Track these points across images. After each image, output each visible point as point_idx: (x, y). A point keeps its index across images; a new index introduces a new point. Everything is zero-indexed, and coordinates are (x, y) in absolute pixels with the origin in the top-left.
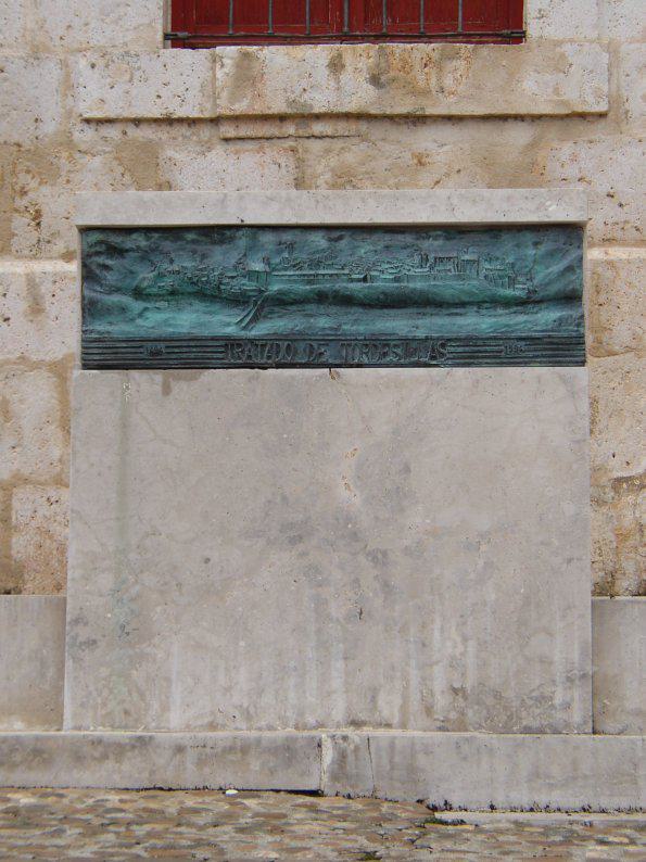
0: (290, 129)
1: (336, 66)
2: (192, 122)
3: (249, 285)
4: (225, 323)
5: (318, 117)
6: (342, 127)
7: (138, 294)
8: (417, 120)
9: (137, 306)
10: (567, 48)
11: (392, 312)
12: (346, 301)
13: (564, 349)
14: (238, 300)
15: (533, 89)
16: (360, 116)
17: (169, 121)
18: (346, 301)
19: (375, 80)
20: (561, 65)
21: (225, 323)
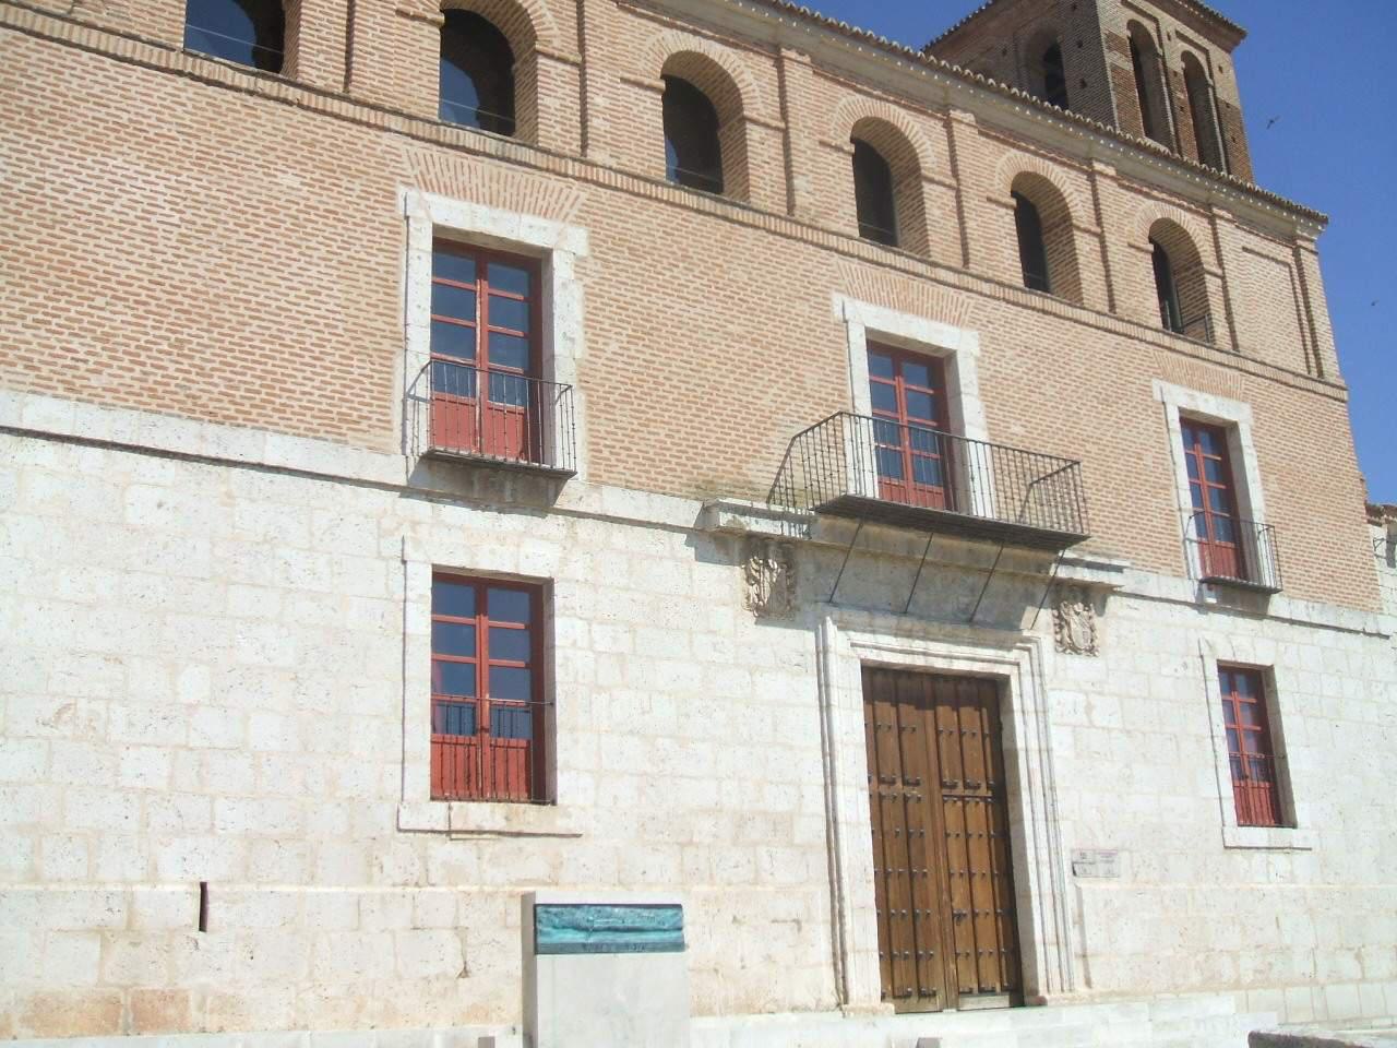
0: (476, 836)
1: (493, 812)
2: (440, 832)
3: (588, 925)
4: (580, 937)
5: (485, 832)
6: (493, 836)
7: (555, 927)
8: (519, 834)
9: (554, 931)
10: (570, 809)
11: (1025, 961)
12: (616, 930)
13: (679, 946)
14: (586, 930)
15: (561, 825)
16: (500, 833)
17: (433, 831)
18: (616, 930)
19: (507, 818)
20: (569, 816)
21: (580, 937)
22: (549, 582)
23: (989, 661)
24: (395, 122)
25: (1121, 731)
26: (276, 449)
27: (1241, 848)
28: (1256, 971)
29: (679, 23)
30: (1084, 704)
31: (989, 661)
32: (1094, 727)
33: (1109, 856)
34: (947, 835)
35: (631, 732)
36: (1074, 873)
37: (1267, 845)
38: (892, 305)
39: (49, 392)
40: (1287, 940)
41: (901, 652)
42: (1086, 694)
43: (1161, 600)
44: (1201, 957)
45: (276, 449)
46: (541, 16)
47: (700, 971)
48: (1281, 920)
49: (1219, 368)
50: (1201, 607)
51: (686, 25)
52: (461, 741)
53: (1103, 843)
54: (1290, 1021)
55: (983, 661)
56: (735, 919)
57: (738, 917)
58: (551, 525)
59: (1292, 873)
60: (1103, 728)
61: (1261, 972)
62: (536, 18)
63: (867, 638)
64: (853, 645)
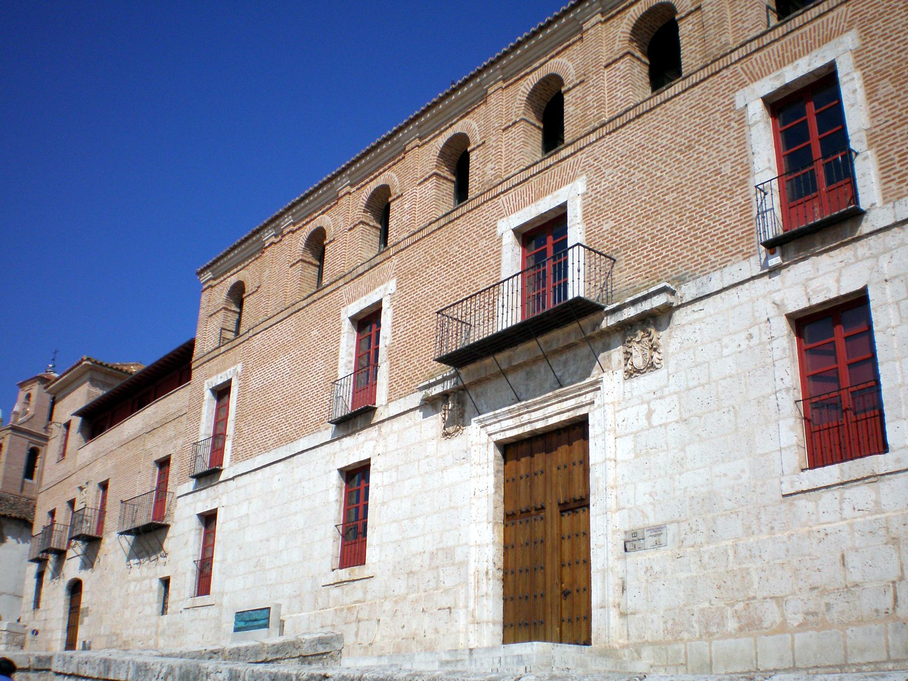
16: (349, 581)
22: (341, 471)
23: (573, 409)
24: (341, 282)
25: (677, 422)
26: (303, 444)
27: (803, 492)
28: (807, 614)
29: (442, 129)
30: (646, 412)
31: (573, 409)
32: (653, 427)
33: (658, 530)
34: (563, 538)
35: (394, 521)
36: (626, 550)
37: (839, 481)
38: (532, 201)
39: (729, 264)
40: (855, 576)
41: (517, 427)
42: (648, 403)
43: (322, 445)
44: (740, 606)
45: (303, 444)
46: (627, 24)
47: (407, 639)
48: (848, 559)
49: (787, 38)
50: (774, 271)
51: (568, 43)
52: (868, 416)
53: (652, 521)
54: (849, 662)
55: (569, 410)
56: (423, 610)
57: (425, 609)
58: (861, 249)
59: (877, 503)
60: (661, 426)
61: (815, 614)
62: (631, 21)
63: (497, 427)
64: (490, 435)
